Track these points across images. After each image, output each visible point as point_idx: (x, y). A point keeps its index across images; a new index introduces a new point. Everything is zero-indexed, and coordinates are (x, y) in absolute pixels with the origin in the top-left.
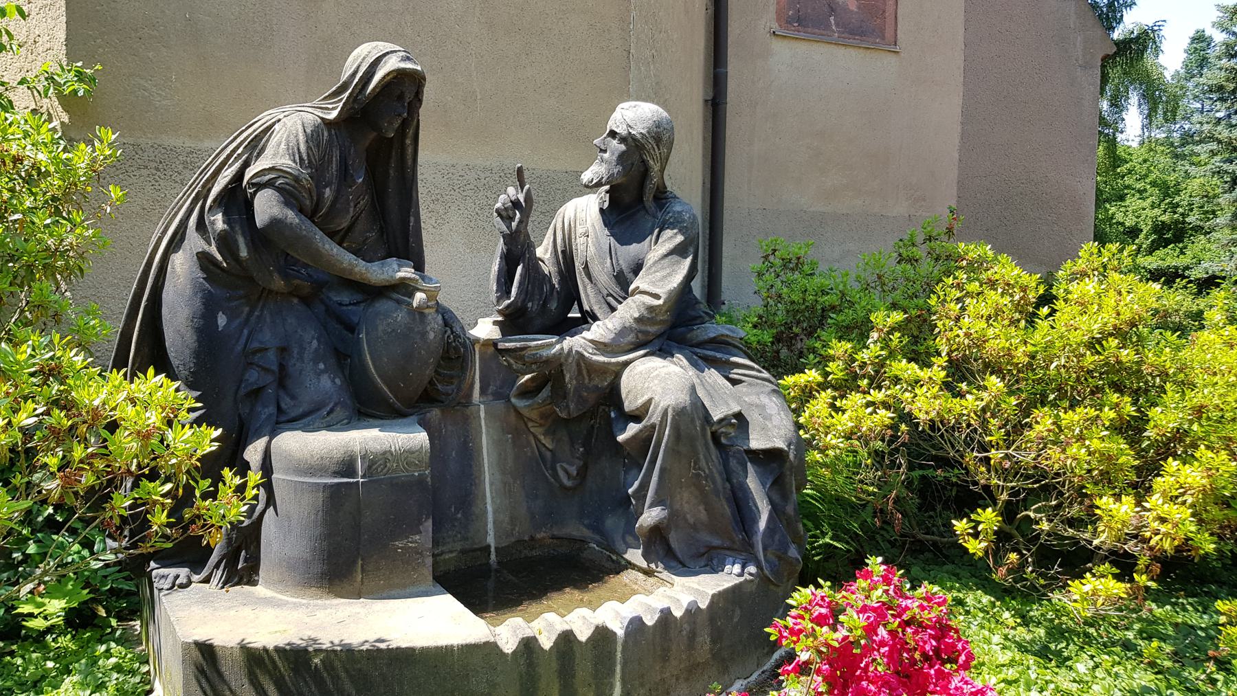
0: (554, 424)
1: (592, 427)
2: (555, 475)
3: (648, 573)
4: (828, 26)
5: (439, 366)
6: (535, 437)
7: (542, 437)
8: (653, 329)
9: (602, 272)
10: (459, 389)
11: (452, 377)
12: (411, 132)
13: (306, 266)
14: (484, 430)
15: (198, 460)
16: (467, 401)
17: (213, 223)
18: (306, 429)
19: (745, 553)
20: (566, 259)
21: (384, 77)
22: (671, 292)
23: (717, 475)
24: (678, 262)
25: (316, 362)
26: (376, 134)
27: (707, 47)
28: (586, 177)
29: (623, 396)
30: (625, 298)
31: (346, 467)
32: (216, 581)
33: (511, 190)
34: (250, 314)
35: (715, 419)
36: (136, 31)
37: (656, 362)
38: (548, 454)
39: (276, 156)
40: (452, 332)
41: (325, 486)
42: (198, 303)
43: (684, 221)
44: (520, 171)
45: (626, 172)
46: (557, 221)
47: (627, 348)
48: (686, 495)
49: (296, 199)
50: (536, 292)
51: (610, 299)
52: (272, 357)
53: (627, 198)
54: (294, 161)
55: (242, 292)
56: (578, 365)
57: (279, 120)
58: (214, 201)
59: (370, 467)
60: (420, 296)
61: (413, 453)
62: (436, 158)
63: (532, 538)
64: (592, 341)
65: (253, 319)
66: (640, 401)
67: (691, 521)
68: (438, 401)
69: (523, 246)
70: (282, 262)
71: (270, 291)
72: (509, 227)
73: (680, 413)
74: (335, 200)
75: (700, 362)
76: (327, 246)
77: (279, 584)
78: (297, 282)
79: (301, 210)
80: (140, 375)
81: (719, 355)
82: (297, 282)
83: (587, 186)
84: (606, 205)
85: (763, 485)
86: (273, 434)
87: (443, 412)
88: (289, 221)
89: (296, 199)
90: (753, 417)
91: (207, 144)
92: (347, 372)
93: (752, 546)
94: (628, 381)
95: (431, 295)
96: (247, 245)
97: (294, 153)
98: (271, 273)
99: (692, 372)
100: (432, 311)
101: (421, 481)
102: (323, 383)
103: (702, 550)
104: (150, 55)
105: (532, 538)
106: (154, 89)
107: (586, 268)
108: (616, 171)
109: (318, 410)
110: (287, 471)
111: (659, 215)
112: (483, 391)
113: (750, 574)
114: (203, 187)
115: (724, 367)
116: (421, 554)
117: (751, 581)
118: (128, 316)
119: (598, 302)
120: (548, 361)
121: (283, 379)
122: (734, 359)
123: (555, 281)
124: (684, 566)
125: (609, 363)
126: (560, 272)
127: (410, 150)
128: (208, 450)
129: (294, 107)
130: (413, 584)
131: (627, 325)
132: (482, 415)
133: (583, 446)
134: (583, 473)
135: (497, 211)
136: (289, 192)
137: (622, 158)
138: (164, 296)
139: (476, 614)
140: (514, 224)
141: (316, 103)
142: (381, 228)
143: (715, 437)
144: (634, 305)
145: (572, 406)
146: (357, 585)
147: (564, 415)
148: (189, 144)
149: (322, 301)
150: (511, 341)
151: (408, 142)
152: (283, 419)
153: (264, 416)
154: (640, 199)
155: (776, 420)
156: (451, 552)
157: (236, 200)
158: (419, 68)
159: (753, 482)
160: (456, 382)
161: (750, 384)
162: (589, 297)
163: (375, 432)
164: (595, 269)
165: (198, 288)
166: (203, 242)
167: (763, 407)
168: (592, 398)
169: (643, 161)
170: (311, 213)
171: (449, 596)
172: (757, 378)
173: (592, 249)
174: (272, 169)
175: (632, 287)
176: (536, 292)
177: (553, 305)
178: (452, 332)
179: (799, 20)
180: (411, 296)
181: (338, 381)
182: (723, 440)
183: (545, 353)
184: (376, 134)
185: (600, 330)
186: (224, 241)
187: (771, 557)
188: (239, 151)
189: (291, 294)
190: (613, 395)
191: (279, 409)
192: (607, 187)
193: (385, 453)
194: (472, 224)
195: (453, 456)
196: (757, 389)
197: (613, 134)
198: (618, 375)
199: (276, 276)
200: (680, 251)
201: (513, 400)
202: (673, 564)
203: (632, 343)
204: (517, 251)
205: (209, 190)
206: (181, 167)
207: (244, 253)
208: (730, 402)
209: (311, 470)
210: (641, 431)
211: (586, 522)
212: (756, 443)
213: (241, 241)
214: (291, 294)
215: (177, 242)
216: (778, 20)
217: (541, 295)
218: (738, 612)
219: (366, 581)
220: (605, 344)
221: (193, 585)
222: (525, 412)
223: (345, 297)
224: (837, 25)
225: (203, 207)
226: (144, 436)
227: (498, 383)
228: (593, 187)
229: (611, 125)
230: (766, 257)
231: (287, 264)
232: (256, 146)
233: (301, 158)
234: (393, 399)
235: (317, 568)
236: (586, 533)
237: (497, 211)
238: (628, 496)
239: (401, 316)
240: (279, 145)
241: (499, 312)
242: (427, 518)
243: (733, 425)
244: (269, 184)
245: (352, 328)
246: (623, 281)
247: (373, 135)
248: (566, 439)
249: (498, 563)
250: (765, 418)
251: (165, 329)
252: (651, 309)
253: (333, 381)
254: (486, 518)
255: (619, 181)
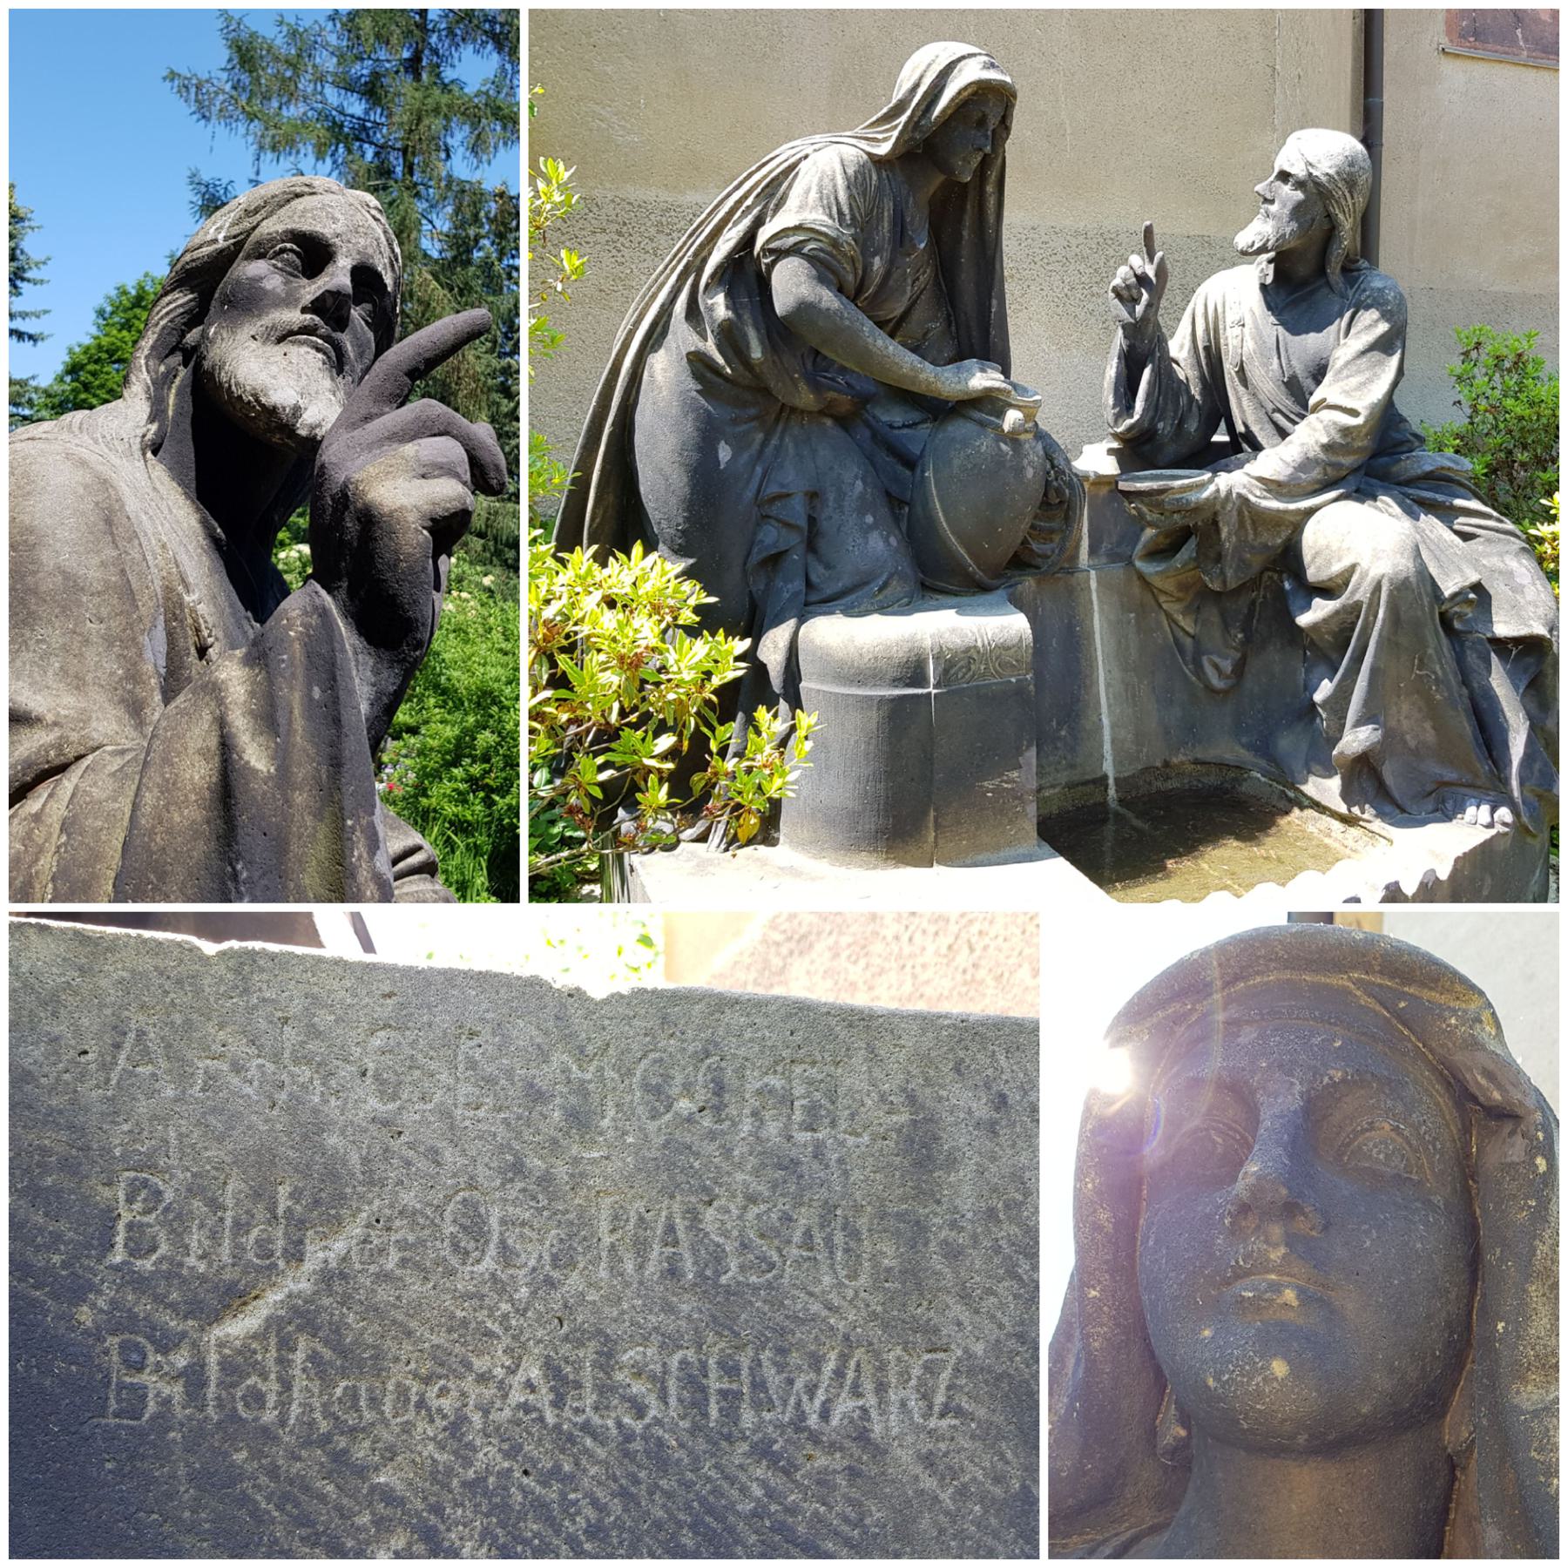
0: (1201, 598)
1: (1253, 603)
2: (1199, 670)
3: (1348, 821)
4: (1514, 41)
5: (1035, 517)
6: (1168, 615)
7: (1180, 618)
8: (1348, 461)
9: (1266, 379)
10: (1062, 550)
11: (1052, 531)
12: (993, 176)
13: (843, 370)
14: (1096, 608)
15: (714, 692)
16: (1071, 568)
17: (711, 309)
18: (849, 612)
19: (1497, 794)
20: (1212, 359)
21: (959, 93)
22: (1373, 407)
23: (1451, 677)
24: (1381, 363)
25: (861, 512)
26: (945, 172)
27: (1354, 70)
28: (1243, 239)
29: (1307, 558)
30: (1303, 417)
31: (913, 672)
32: (717, 840)
33: (1136, 261)
34: (764, 444)
35: (1447, 594)
36: (589, 35)
37: (1352, 510)
38: (1188, 642)
39: (803, 208)
40: (1053, 467)
41: (882, 700)
42: (689, 427)
43: (1387, 302)
44: (1148, 231)
45: (1303, 230)
46: (1197, 302)
47: (1311, 488)
48: (1405, 707)
49: (834, 272)
50: (1170, 407)
51: (1278, 417)
52: (797, 509)
53: (1303, 270)
54: (831, 216)
55: (753, 411)
56: (1240, 513)
57: (806, 157)
58: (712, 276)
59: (946, 671)
60: (1012, 417)
61: (1009, 648)
62: (1034, 218)
63: (1167, 764)
64: (1260, 479)
65: (769, 450)
66: (1337, 568)
67: (1412, 743)
68: (1030, 566)
69: (1151, 342)
70: (809, 366)
71: (793, 410)
72: (1132, 313)
73: (1401, 587)
74: (887, 275)
75: (1416, 507)
76: (880, 343)
77: (813, 845)
78: (832, 395)
79: (840, 290)
80: (619, 554)
81: (1440, 498)
82: (832, 395)
83: (1244, 253)
84: (1269, 280)
85: (1516, 688)
86: (802, 620)
87: (1038, 583)
88: (824, 305)
89: (834, 272)
90: (1496, 589)
91: (691, 197)
92: (904, 527)
93: (1506, 782)
94: (1314, 537)
95: (1030, 412)
96: (762, 343)
97: (829, 203)
98: (794, 382)
99: (1406, 523)
100: (1030, 436)
101: (1019, 691)
102: (871, 544)
103: (1429, 788)
104: (609, 69)
105: (1167, 764)
106: (614, 119)
107: (1241, 372)
108: (1288, 230)
109: (866, 583)
110: (822, 677)
111: (1350, 293)
112: (1093, 551)
113: (1505, 824)
114: (696, 255)
115: (1447, 514)
116: (1020, 798)
117: (1506, 834)
118: (584, 447)
119: (1259, 421)
120: (1198, 509)
121: (813, 538)
122: (1458, 502)
123: (1195, 391)
124: (1403, 811)
125: (1286, 512)
126: (1202, 378)
127: (992, 201)
128: (731, 675)
129: (827, 137)
130: (1009, 844)
131: (1311, 455)
132: (1093, 585)
133: (1243, 631)
134: (1240, 669)
135: (1115, 290)
136: (824, 266)
137: (1298, 211)
138: (638, 417)
139: (1101, 885)
140: (1139, 309)
141: (858, 131)
142: (949, 315)
143: (1446, 621)
144: (1320, 426)
145: (1229, 573)
146: (928, 847)
147: (1216, 586)
148: (665, 196)
149: (869, 426)
150: (1146, 479)
151: (990, 189)
152: (813, 598)
153: (786, 595)
154: (1321, 270)
155: (1530, 593)
156: (1053, 786)
157: (745, 274)
158: (1008, 79)
159: (1500, 682)
160: (1057, 538)
161: (1489, 540)
162: (1243, 410)
163: (949, 615)
164: (1255, 373)
165: (689, 407)
166: (696, 337)
167: (1511, 574)
168: (1257, 562)
169: (1329, 216)
170: (852, 293)
171: (1061, 860)
172: (1497, 531)
173: (1250, 345)
174: (799, 228)
175: (1312, 401)
176: (1170, 407)
177: (1192, 426)
178: (1053, 467)
179: (1476, 34)
180: (1000, 414)
181: (893, 540)
182: (1457, 625)
183: (1193, 497)
184: (945, 172)
185: (1275, 460)
186: (729, 337)
187: (1531, 797)
188: (749, 202)
189: (822, 413)
190: (1289, 558)
191: (809, 584)
192: (1272, 254)
193: (968, 650)
194: (1059, 311)
195: (1060, 643)
196: (1500, 547)
197: (1284, 176)
198: (1298, 528)
199: (802, 386)
200: (1384, 345)
201: (1138, 564)
202: (1388, 808)
203: (1318, 482)
204: (1142, 348)
205: (705, 261)
206: (653, 231)
207: (756, 353)
208: (1464, 567)
209: (861, 676)
210: (1337, 613)
211: (1244, 740)
212: (1503, 627)
213: (752, 334)
214: (822, 413)
215: (656, 337)
216: (1449, 32)
217: (1176, 412)
218: (1489, 881)
219: (941, 842)
220: (1279, 484)
221: (682, 845)
222: (1157, 582)
223: (895, 415)
224: (1526, 40)
225: (695, 286)
226: (631, 663)
227: (1114, 539)
228: (1248, 254)
229: (1282, 162)
230: (1466, 354)
231: (817, 365)
232: (773, 193)
233: (840, 212)
234: (973, 568)
235: (870, 824)
236: (1244, 755)
237: (1115, 290)
238: (1314, 704)
239: (985, 444)
240: (808, 192)
241: (1116, 436)
242: (1028, 747)
243: (1471, 602)
244: (794, 250)
245: (911, 463)
246: (1299, 392)
247: (941, 178)
248: (1216, 619)
249: (1120, 801)
250: (1514, 590)
251: (640, 466)
252: (1346, 431)
253: (886, 541)
254: (1102, 736)
255: (1292, 244)
